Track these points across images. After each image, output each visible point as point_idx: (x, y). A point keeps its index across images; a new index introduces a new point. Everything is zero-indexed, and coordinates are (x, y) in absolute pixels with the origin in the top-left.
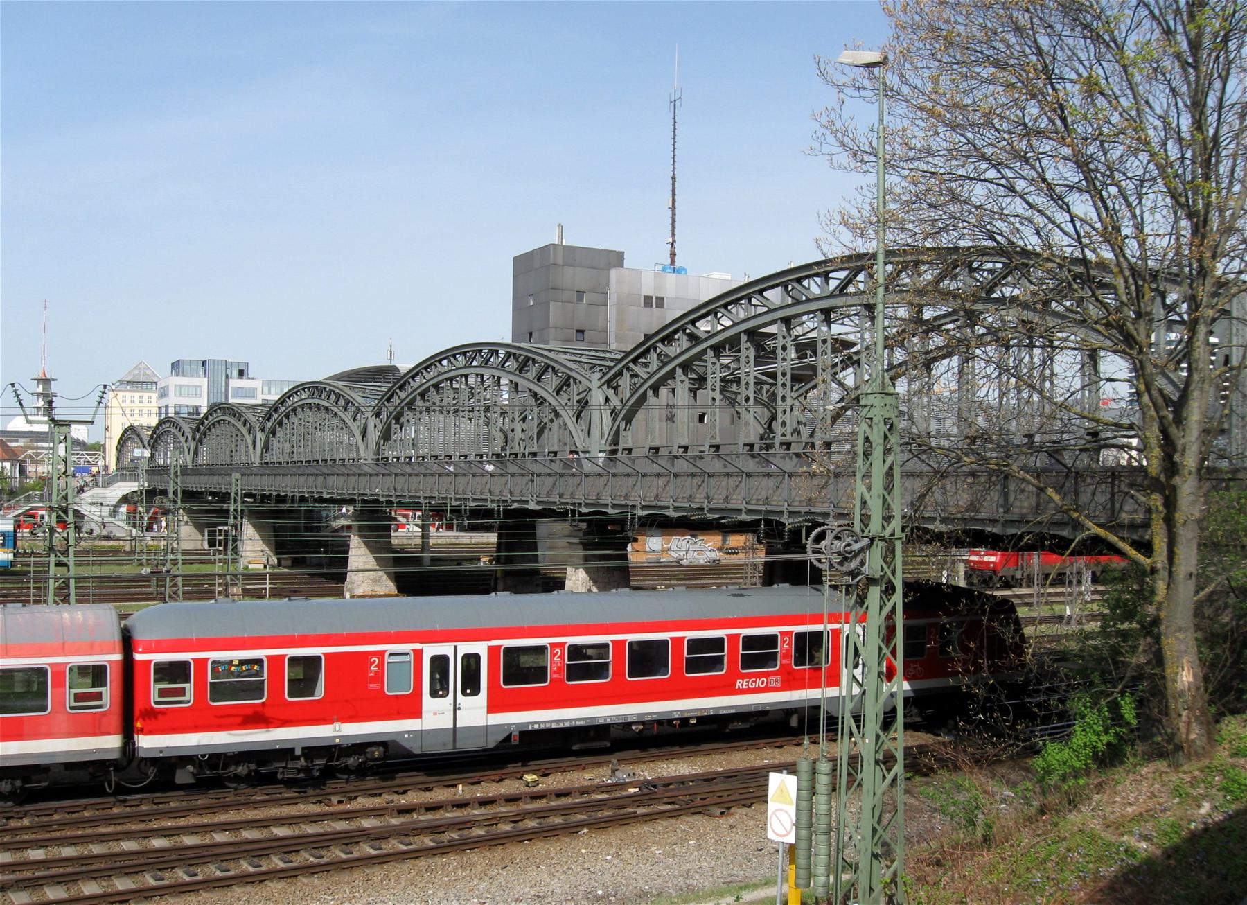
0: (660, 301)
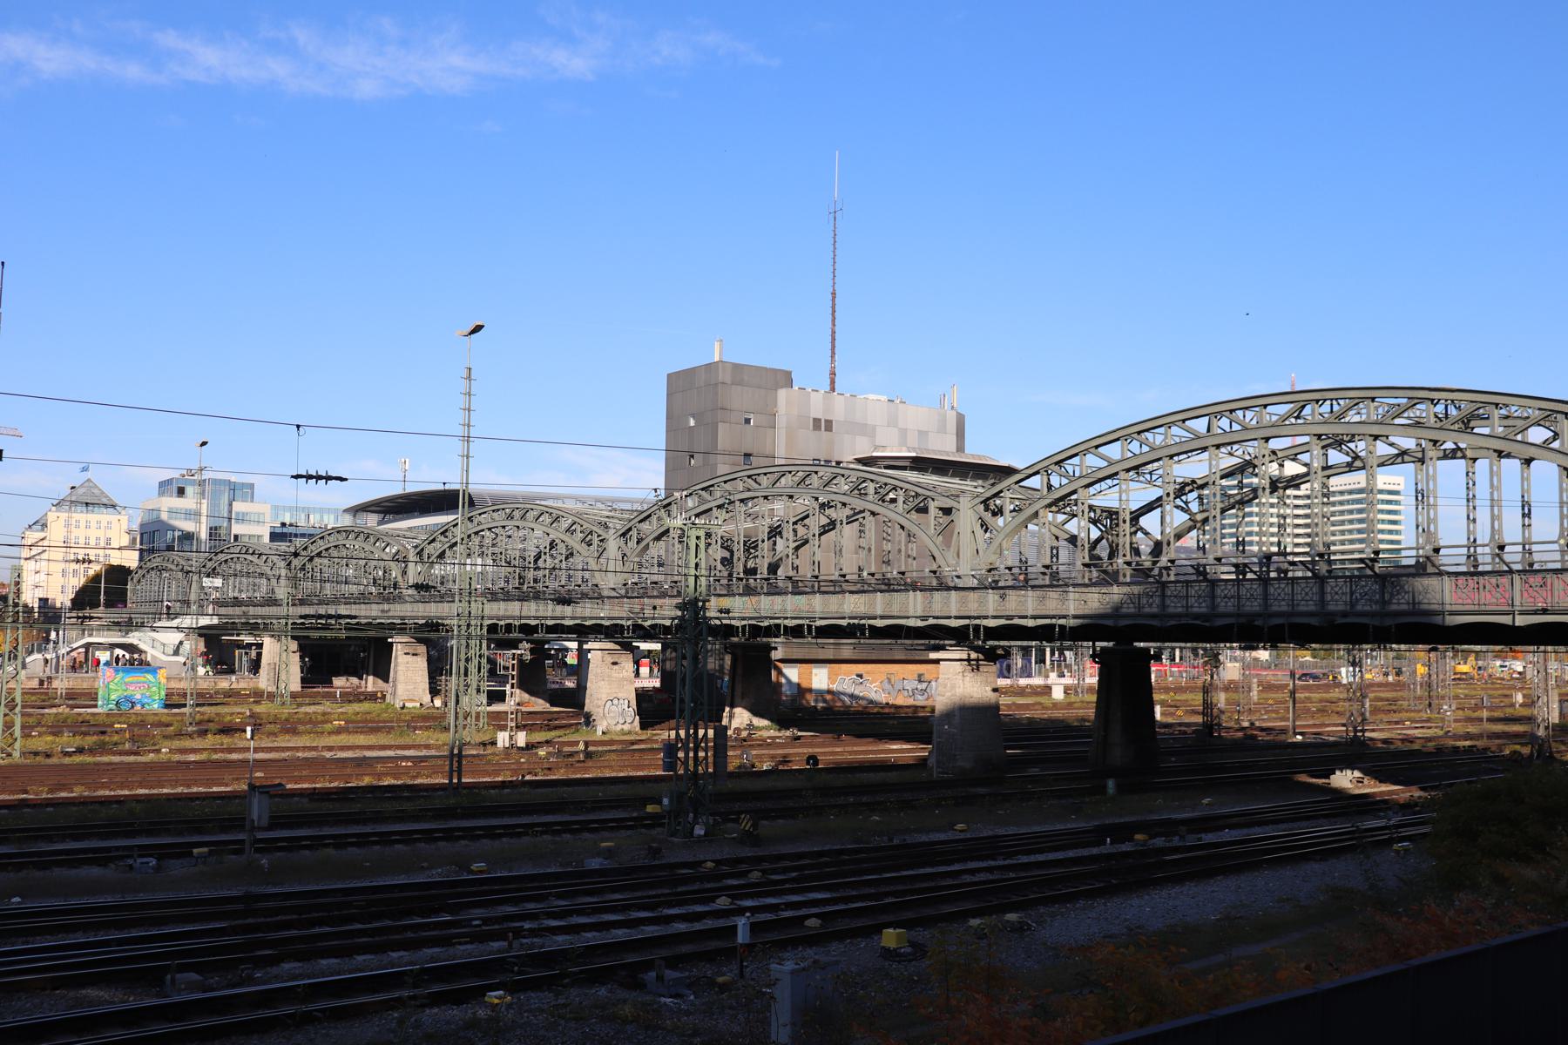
0: (829, 425)
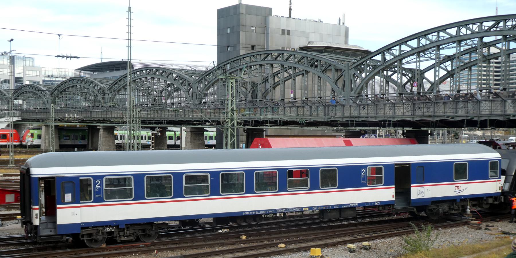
0: (289, 32)
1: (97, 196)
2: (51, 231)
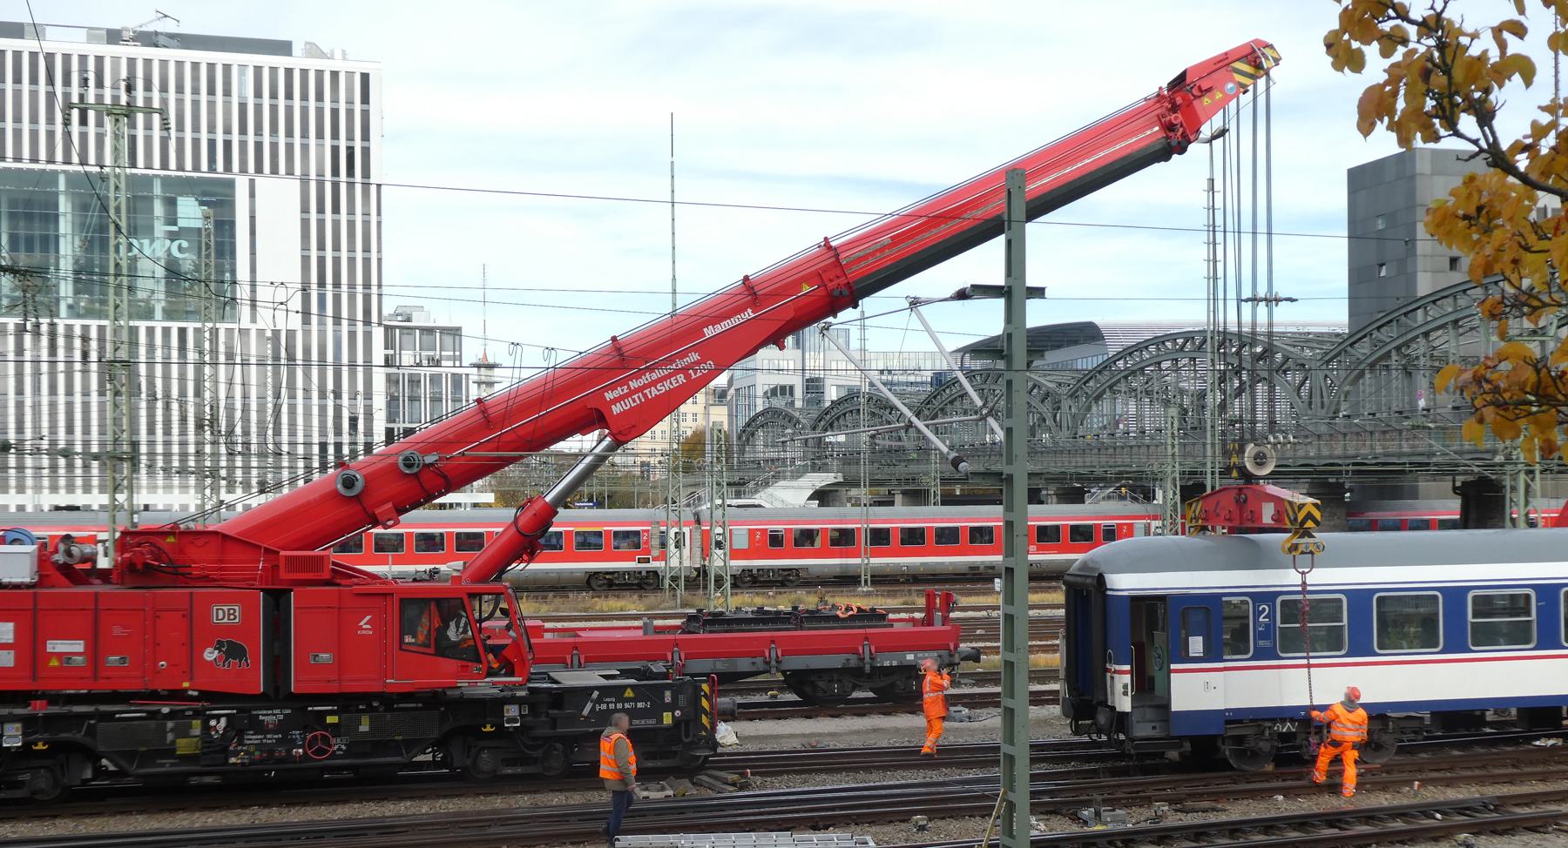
1: (1261, 643)
2: (1154, 728)
